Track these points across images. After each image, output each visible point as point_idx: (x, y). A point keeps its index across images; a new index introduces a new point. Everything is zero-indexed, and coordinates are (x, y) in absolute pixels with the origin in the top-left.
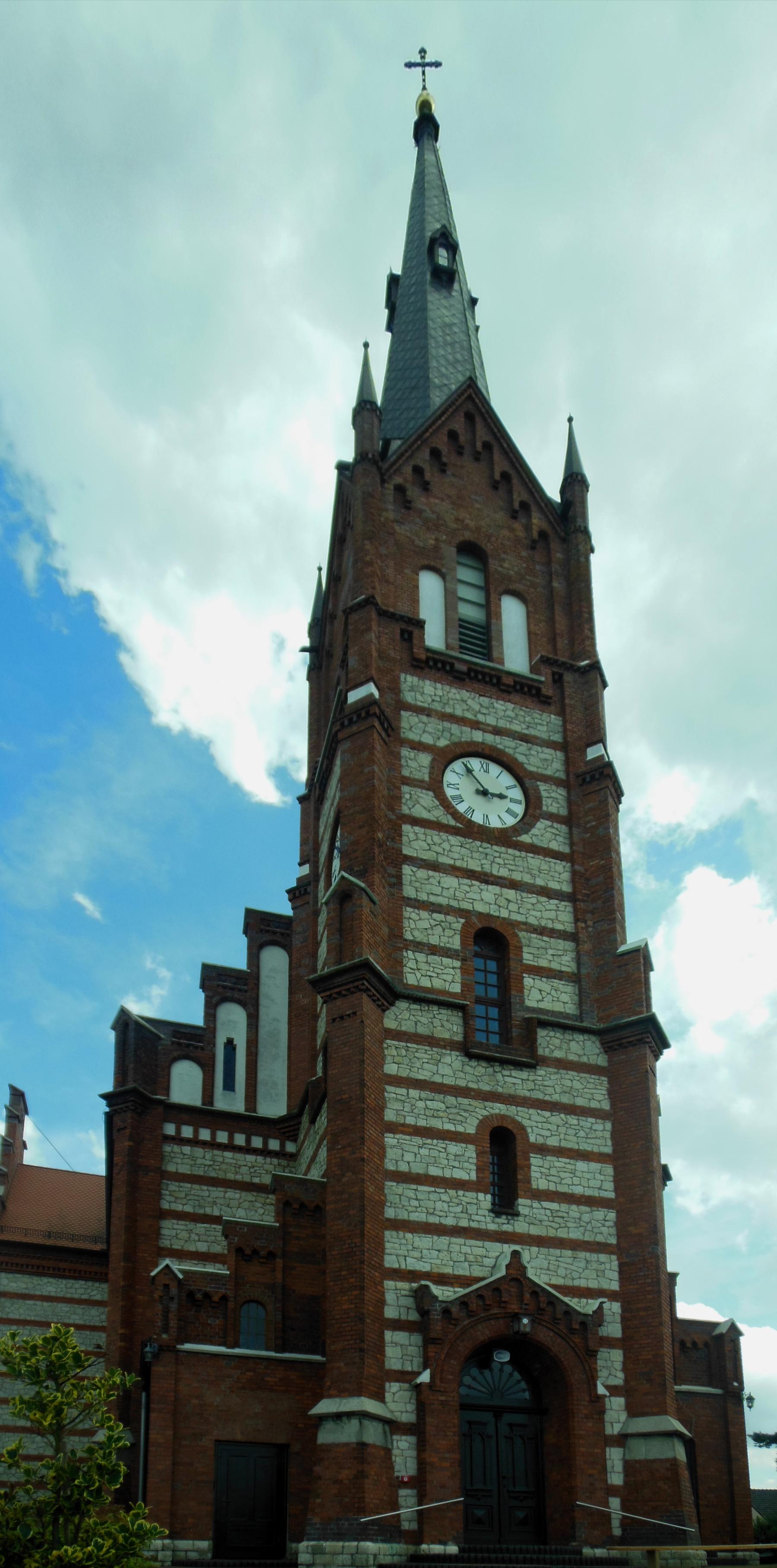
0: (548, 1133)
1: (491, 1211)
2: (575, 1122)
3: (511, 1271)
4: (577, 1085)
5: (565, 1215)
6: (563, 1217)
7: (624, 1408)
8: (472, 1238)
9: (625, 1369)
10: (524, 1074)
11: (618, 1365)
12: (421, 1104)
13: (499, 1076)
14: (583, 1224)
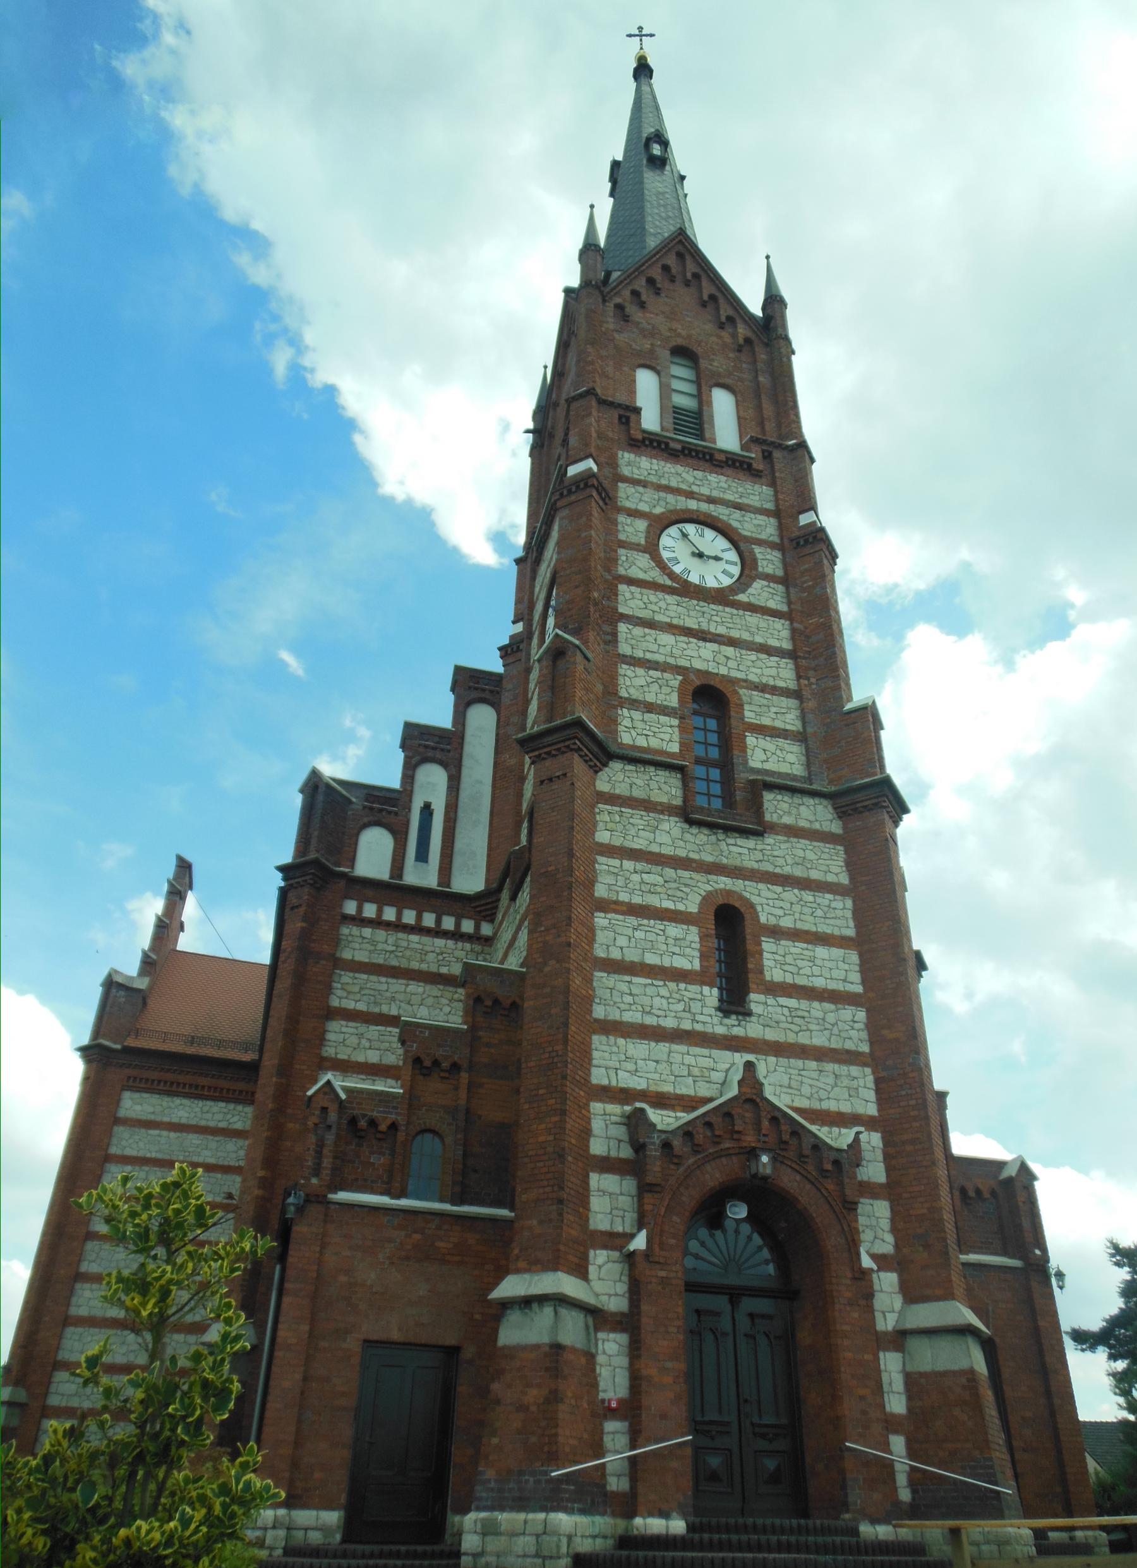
0: (780, 912)
1: (719, 1009)
2: (811, 899)
3: (744, 1090)
4: (810, 855)
5: (806, 1014)
6: (804, 1018)
7: (897, 1289)
8: (696, 1045)
9: (894, 1230)
10: (751, 843)
11: (885, 1224)
12: (636, 878)
13: (723, 845)
14: (828, 1026)
